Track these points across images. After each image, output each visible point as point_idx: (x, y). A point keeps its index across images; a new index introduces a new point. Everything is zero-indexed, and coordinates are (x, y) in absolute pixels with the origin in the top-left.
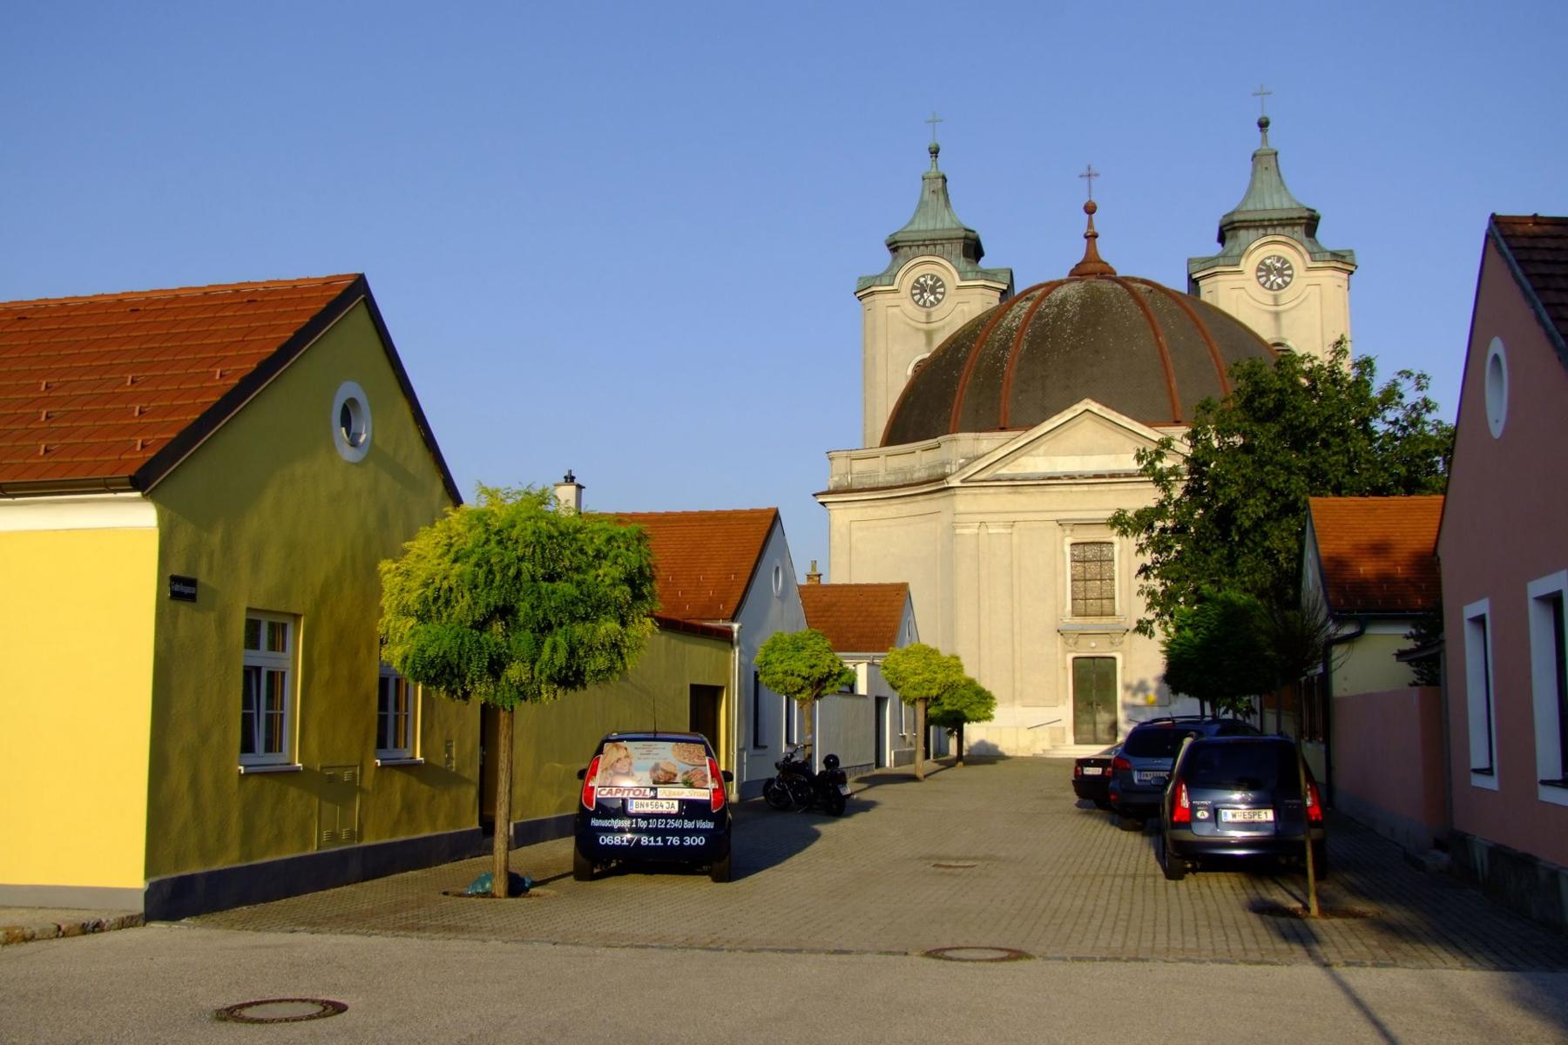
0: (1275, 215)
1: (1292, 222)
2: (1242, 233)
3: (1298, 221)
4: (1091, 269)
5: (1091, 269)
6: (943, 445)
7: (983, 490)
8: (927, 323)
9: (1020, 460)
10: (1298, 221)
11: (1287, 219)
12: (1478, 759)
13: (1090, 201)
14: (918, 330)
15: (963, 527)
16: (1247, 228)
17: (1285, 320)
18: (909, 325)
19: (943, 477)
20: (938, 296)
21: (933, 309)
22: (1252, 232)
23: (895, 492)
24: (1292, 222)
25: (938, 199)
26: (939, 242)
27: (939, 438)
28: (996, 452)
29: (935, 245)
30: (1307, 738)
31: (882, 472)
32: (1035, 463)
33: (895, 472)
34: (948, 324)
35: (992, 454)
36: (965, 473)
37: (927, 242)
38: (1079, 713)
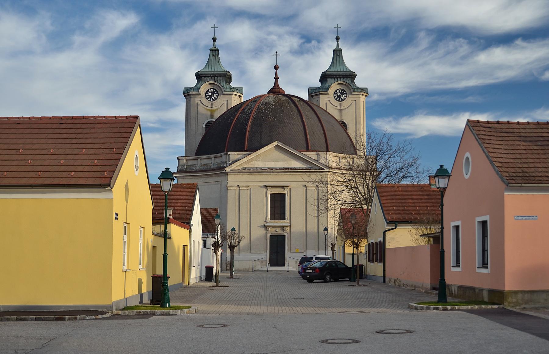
0: (341, 73)
1: (347, 76)
2: (329, 79)
3: (349, 76)
4: (276, 90)
5: (276, 90)
8: (211, 107)
10: (349, 76)
11: (345, 75)
15: (230, 187)
16: (331, 78)
17: (343, 112)
18: (204, 108)
21: (213, 102)
22: (333, 80)
23: (204, 173)
24: (347, 76)
25: (215, 59)
27: (222, 153)
31: (199, 165)
32: (260, 164)
33: (204, 165)
36: (231, 167)
37: (212, 76)
38: (272, 255)
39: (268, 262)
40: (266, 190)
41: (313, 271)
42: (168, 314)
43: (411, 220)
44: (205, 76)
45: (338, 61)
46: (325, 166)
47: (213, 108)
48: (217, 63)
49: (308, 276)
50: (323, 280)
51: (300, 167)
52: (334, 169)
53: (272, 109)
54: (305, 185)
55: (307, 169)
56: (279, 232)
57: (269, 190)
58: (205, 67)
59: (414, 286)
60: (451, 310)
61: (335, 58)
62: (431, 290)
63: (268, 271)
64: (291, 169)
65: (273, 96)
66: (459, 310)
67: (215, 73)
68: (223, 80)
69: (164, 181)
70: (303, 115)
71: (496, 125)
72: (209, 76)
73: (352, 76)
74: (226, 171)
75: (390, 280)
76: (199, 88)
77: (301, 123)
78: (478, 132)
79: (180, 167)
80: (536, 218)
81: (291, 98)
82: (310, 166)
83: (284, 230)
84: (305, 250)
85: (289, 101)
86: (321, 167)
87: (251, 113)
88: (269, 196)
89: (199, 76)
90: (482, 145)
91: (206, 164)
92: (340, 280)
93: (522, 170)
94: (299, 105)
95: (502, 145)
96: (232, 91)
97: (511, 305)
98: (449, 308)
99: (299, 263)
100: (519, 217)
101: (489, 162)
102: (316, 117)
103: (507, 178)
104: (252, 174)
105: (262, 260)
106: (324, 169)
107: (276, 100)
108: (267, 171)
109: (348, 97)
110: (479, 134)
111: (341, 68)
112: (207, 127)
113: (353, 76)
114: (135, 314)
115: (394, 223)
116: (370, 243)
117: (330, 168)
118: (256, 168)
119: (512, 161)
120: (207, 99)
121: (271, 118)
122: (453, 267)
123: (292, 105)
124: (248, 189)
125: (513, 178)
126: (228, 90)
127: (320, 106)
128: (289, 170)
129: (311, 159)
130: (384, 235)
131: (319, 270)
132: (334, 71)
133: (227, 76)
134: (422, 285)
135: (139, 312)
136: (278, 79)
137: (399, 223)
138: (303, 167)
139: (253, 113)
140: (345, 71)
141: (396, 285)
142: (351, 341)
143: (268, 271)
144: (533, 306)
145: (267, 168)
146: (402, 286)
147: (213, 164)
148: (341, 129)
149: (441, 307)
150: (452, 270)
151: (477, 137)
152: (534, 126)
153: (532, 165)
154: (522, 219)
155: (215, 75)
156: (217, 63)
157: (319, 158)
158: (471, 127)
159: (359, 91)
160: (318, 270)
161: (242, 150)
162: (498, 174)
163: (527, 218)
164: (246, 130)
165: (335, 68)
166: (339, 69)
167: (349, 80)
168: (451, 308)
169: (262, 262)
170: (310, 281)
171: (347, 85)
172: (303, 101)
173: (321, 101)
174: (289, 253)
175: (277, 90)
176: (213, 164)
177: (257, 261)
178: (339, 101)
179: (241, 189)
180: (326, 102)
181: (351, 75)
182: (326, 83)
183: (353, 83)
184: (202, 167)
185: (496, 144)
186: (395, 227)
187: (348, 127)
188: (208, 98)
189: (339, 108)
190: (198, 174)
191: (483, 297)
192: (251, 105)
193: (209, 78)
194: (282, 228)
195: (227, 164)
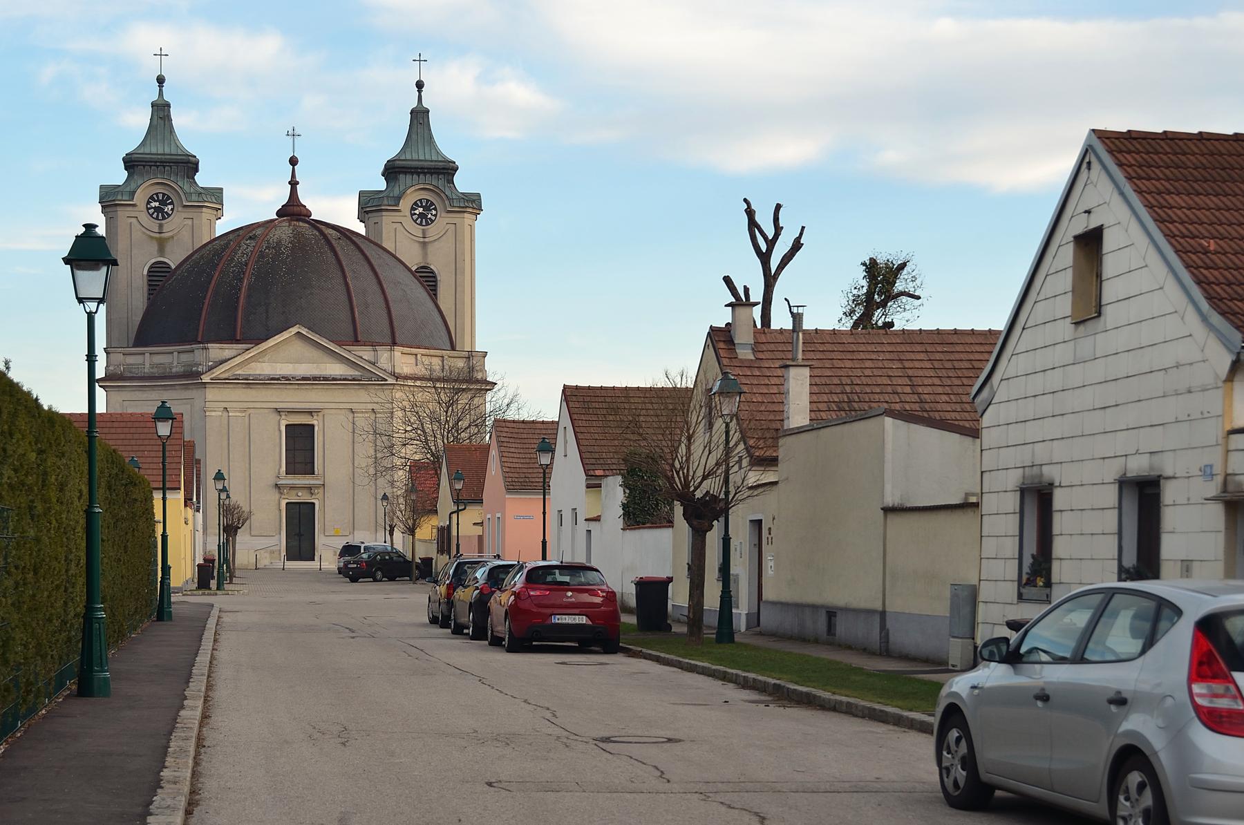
0: (426, 164)
1: (438, 171)
2: (402, 177)
3: (442, 171)
4: (293, 210)
5: (293, 210)
6: (196, 351)
7: (226, 386)
10: (442, 171)
11: (434, 169)
15: (211, 411)
16: (405, 173)
17: (430, 248)
19: (198, 374)
21: (163, 222)
22: (409, 177)
24: (438, 171)
25: (164, 125)
26: (168, 164)
27: (193, 346)
28: (236, 359)
29: (164, 167)
31: (147, 365)
32: (264, 368)
33: (158, 365)
34: (176, 234)
35: (233, 360)
36: (213, 373)
37: (158, 164)
38: (289, 540)
39: (284, 553)
40: (279, 417)
46: (388, 375)
48: (167, 134)
49: (351, 573)
50: (371, 579)
51: (341, 375)
55: (354, 380)
56: (304, 497)
57: (283, 417)
58: (143, 143)
61: (414, 130)
63: (283, 569)
64: (325, 379)
68: (183, 174)
74: (203, 381)
79: (111, 368)
82: (360, 374)
83: (312, 494)
84: (352, 531)
85: (319, 239)
87: (246, 265)
88: (283, 429)
89: (131, 163)
91: (161, 364)
94: (338, 249)
96: (201, 199)
99: (339, 555)
102: (371, 273)
103: (509, 484)
104: (251, 386)
106: (386, 380)
107: (293, 236)
108: (279, 382)
109: (440, 217)
112: (151, 274)
113: (449, 171)
117: (398, 378)
118: (260, 375)
120: (151, 215)
123: (326, 248)
124: (244, 415)
126: (194, 197)
127: (384, 245)
128: (320, 380)
129: (361, 360)
131: (366, 565)
132: (412, 160)
133: (189, 165)
138: (348, 375)
139: (251, 263)
143: (283, 569)
145: (280, 375)
147: (175, 364)
148: (420, 293)
155: (166, 162)
156: (167, 134)
157: (376, 357)
161: (233, 340)
164: (238, 298)
166: (421, 155)
167: (443, 180)
169: (272, 552)
170: (354, 580)
171: (436, 191)
173: (383, 224)
174: (322, 536)
175: (296, 209)
176: (175, 364)
177: (262, 551)
178: (421, 224)
179: (230, 414)
180: (395, 225)
182: (394, 185)
184: (155, 370)
187: (439, 279)
188: (153, 213)
190: (147, 384)
194: (310, 489)
195: (205, 367)
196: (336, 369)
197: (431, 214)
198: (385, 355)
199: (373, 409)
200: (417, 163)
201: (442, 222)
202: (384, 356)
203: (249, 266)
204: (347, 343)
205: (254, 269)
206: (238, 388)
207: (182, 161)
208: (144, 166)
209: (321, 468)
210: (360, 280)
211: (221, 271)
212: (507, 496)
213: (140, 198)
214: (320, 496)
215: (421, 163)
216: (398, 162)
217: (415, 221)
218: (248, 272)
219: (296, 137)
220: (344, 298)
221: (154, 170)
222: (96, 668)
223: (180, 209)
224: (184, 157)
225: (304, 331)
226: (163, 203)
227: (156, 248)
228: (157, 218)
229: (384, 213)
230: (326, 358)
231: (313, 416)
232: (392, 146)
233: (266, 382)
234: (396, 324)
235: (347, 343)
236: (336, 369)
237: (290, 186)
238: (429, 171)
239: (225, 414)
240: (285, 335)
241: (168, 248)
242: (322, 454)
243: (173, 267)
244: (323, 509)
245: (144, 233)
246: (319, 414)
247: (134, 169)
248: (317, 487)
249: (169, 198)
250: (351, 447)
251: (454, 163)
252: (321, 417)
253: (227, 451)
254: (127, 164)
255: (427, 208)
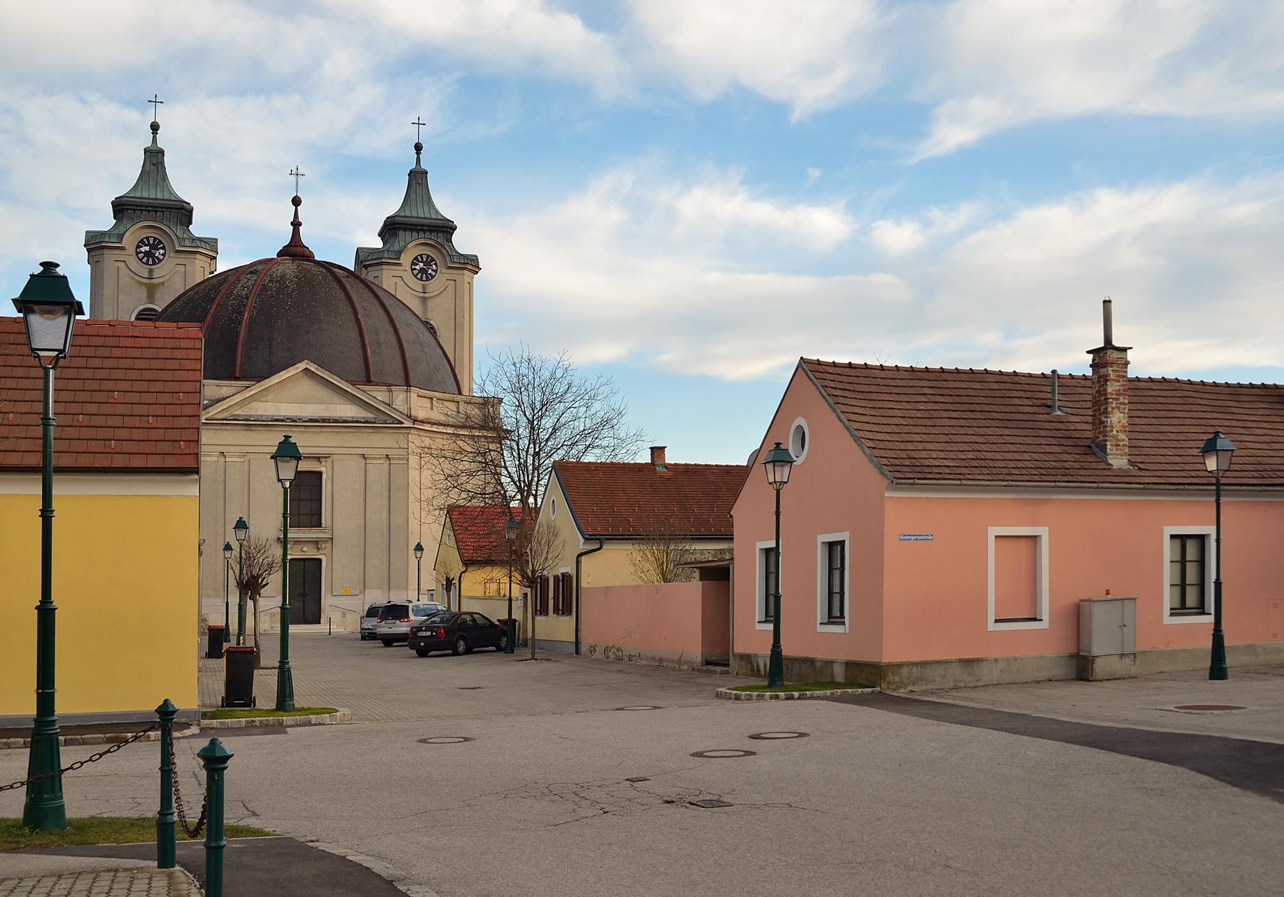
0: (426, 222)
1: (438, 229)
2: (401, 233)
3: (441, 229)
4: (295, 250)
5: (295, 250)
9: (252, 404)
10: (441, 229)
11: (434, 226)
12: (343, 630)
13: (297, 196)
14: (141, 283)
16: (405, 230)
17: (430, 304)
20: (142, 255)
21: (154, 267)
22: (408, 234)
24: (438, 229)
25: (157, 171)
28: (235, 397)
29: (156, 212)
30: (49, 605)
34: (167, 281)
36: (209, 413)
37: (150, 209)
41: (432, 633)
42: (309, 724)
43: (628, 533)
44: (135, 208)
45: (420, 196)
46: (405, 417)
47: (153, 281)
51: (353, 418)
52: (422, 422)
53: (293, 291)
54: (364, 455)
55: (367, 422)
56: (309, 552)
58: (134, 188)
59: (657, 659)
60: (799, 698)
61: (413, 189)
62: (702, 665)
64: (335, 421)
65: (293, 263)
66: (811, 698)
67: (157, 203)
69: (283, 461)
70: (357, 306)
71: (847, 369)
72: (144, 208)
73: (447, 229)
75: (593, 649)
76: (123, 235)
77: (353, 324)
78: (824, 383)
80: (932, 538)
81: (333, 272)
82: (373, 416)
83: (318, 549)
84: (362, 589)
86: (397, 417)
87: (247, 298)
90: (835, 407)
92: (395, 644)
93: (908, 455)
94: (348, 286)
95: (866, 407)
97: (891, 687)
98: (796, 694)
100: (905, 536)
101: (851, 439)
102: (382, 312)
105: (272, 610)
106: (403, 423)
108: (284, 423)
109: (441, 273)
110: (827, 387)
111: (425, 210)
113: (449, 230)
114: (244, 725)
115: (598, 539)
116: (560, 575)
118: (262, 416)
119: (888, 437)
120: (141, 260)
121: (290, 310)
122: (758, 622)
123: (335, 284)
124: (243, 460)
125: (899, 469)
126: (187, 243)
127: (384, 287)
130: (578, 562)
134: (681, 657)
135: (252, 721)
136: (301, 225)
137: (607, 539)
138: (370, 418)
139: (252, 297)
140: (433, 217)
141: (608, 657)
142: (743, 753)
144: (924, 688)
146: (626, 659)
149: (782, 693)
150: (757, 628)
151: (823, 391)
152: (907, 375)
153: (920, 446)
154: (910, 539)
155: (158, 207)
157: (391, 398)
158: (809, 372)
159: (462, 261)
160: (442, 631)
161: (231, 376)
162: (871, 461)
163: (917, 538)
164: (238, 333)
165: (412, 209)
166: (420, 213)
167: (442, 238)
168: (800, 695)
172: (356, 278)
174: (329, 595)
175: (299, 249)
181: (447, 227)
183: (450, 244)
185: (857, 406)
186: (598, 547)
188: (143, 258)
189: (422, 295)
191: (832, 674)
192: (246, 280)
193: (144, 212)
194: (316, 543)
196: (348, 411)
197: (432, 270)
198: (401, 396)
199: (387, 455)
200: (416, 220)
201: (442, 278)
202: (399, 397)
203: (250, 299)
204: (359, 383)
205: (255, 303)
206: (237, 430)
207: (176, 207)
208: (134, 210)
209: (329, 520)
210: (373, 319)
211: (219, 305)
212: (888, 494)
213: (129, 241)
214: (328, 551)
215: (420, 220)
216: (398, 218)
217: (416, 276)
218: (249, 304)
219: (300, 178)
220: (355, 334)
221: (145, 215)
222: (46, 796)
223: (172, 254)
224: (177, 203)
225: (313, 368)
226: (154, 247)
227: (145, 294)
228: (147, 263)
229: (384, 267)
230: (336, 398)
231: (320, 462)
232: (392, 204)
233: (269, 423)
234: (409, 366)
235: (359, 383)
236: (348, 411)
237: (292, 227)
238: (429, 228)
239: (222, 459)
240: (292, 371)
241: (158, 296)
242: (330, 504)
243: (160, 310)
244: (330, 565)
245: (132, 278)
246: (328, 460)
247: (123, 213)
248: (325, 541)
249: (160, 242)
250: (363, 496)
251: (453, 222)
252: (329, 464)
253: (222, 502)
254: (116, 209)
255: (427, 264)
